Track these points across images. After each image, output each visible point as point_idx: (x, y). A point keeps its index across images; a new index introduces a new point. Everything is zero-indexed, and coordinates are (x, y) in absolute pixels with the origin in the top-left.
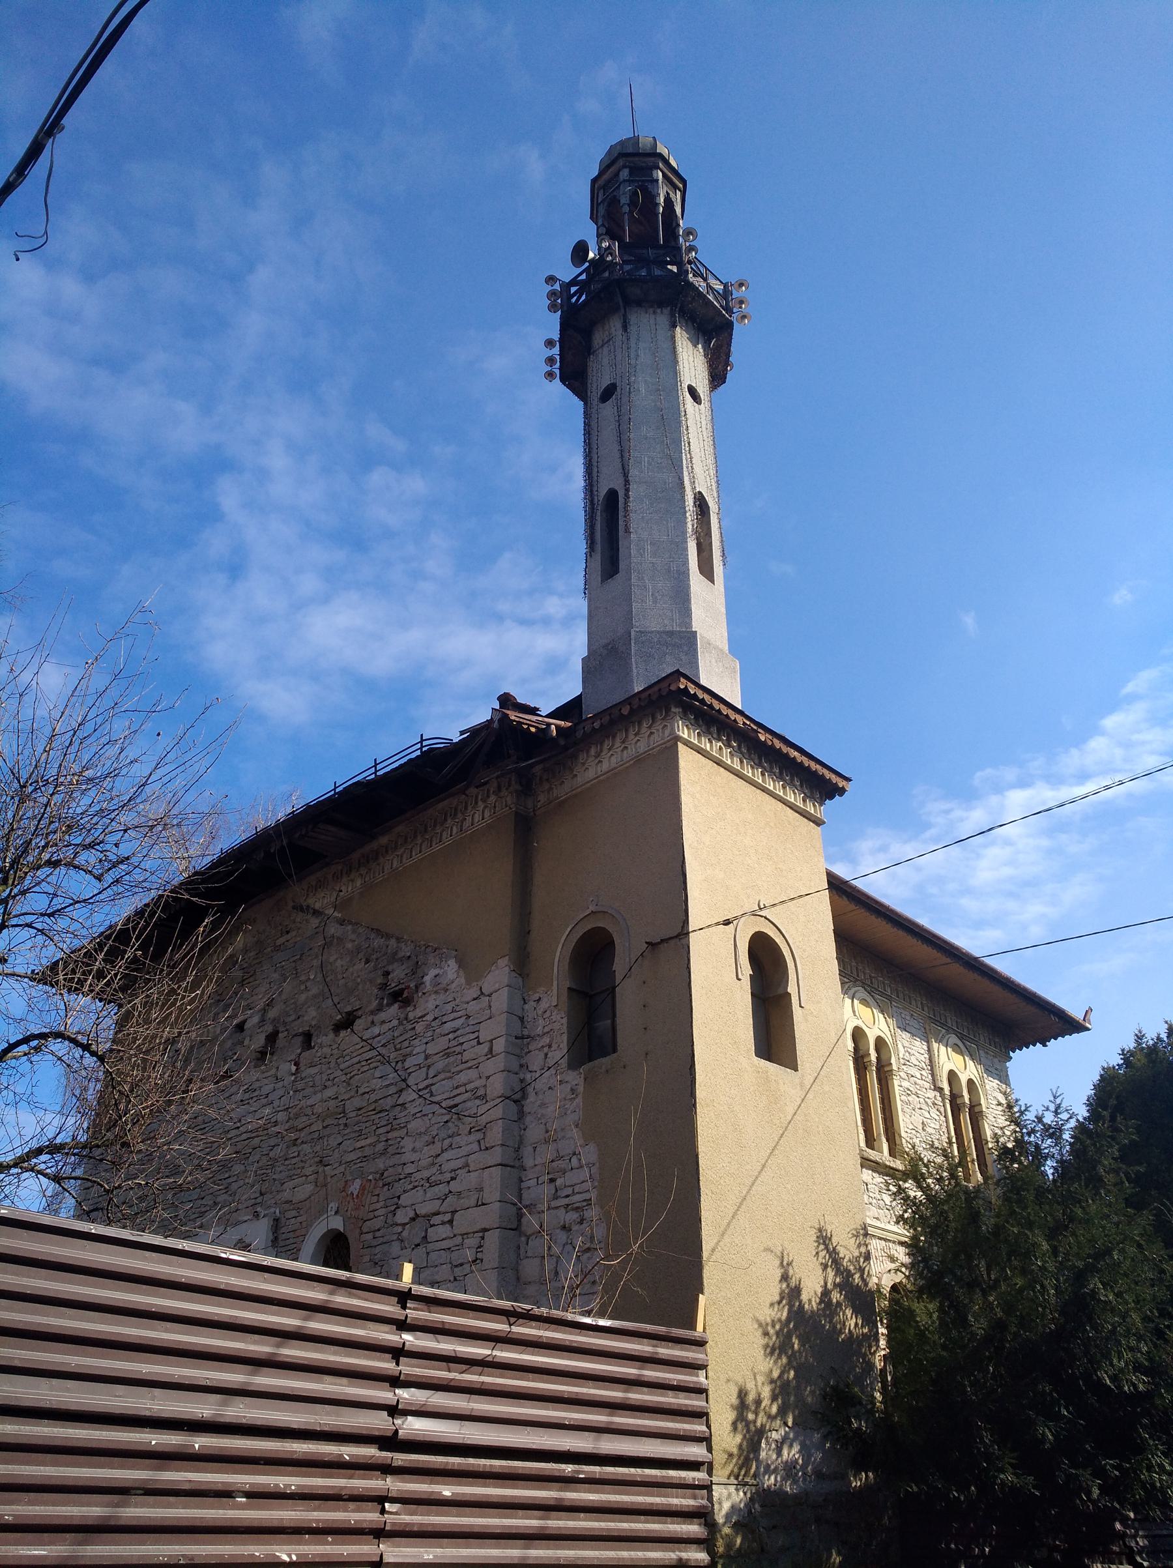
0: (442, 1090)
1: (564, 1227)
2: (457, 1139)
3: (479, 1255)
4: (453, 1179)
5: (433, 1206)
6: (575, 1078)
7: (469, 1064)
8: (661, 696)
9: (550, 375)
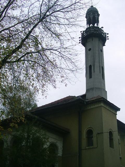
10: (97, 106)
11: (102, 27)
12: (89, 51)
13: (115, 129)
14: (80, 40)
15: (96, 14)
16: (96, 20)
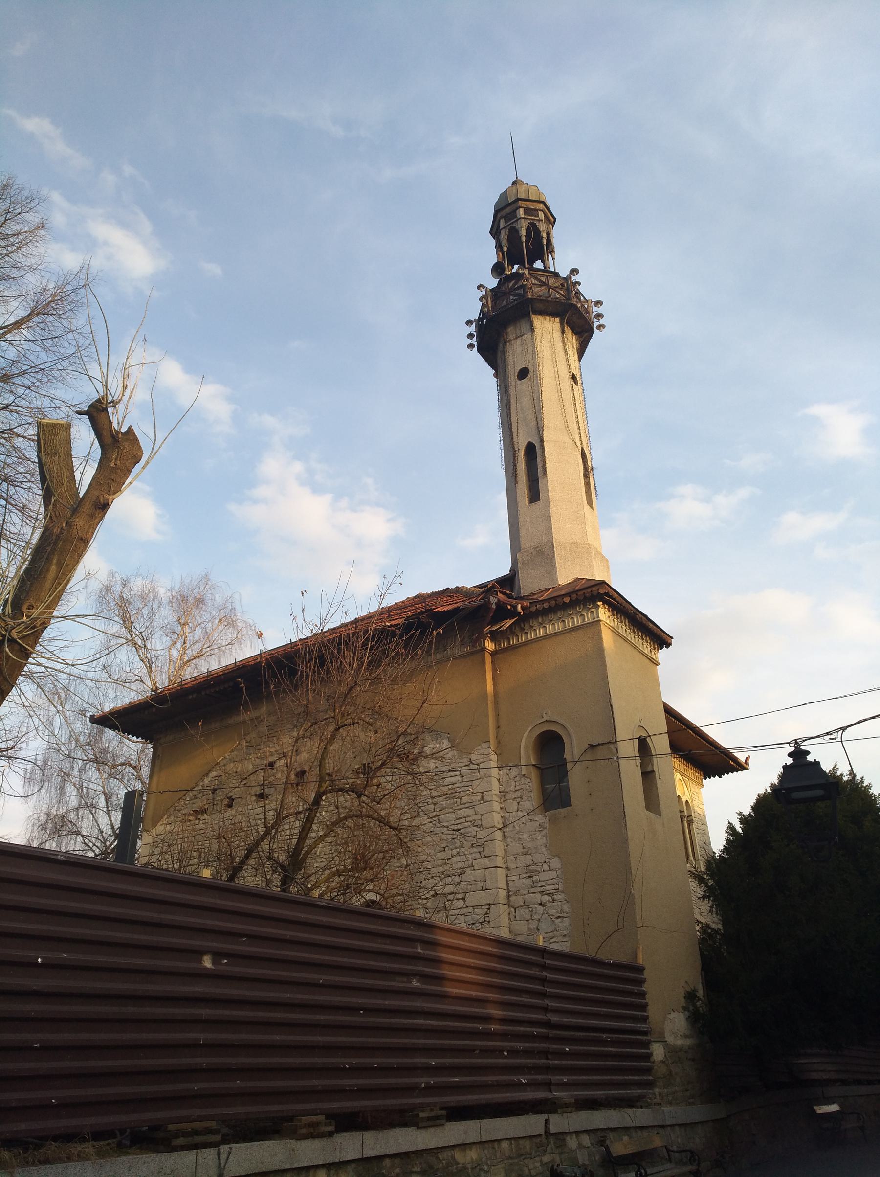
0: (449, 818)
1: (541, 904)
2: (463, 850)
3: (487, 919)
4: (462, 873)
5: (450, 889)
6: (539, 818)
7: (467, 805)
8: (585, 598)
9: (471, 346)
10: (577, 621)
11: (574, 271)
12: (525, 368)
13: (659, 725)
14: (470, 336)
15: (541, 215)
16: (545, 242)
